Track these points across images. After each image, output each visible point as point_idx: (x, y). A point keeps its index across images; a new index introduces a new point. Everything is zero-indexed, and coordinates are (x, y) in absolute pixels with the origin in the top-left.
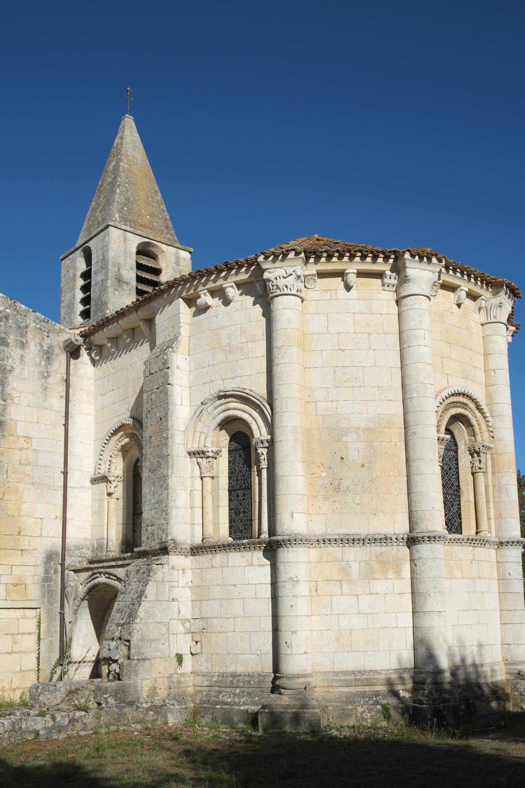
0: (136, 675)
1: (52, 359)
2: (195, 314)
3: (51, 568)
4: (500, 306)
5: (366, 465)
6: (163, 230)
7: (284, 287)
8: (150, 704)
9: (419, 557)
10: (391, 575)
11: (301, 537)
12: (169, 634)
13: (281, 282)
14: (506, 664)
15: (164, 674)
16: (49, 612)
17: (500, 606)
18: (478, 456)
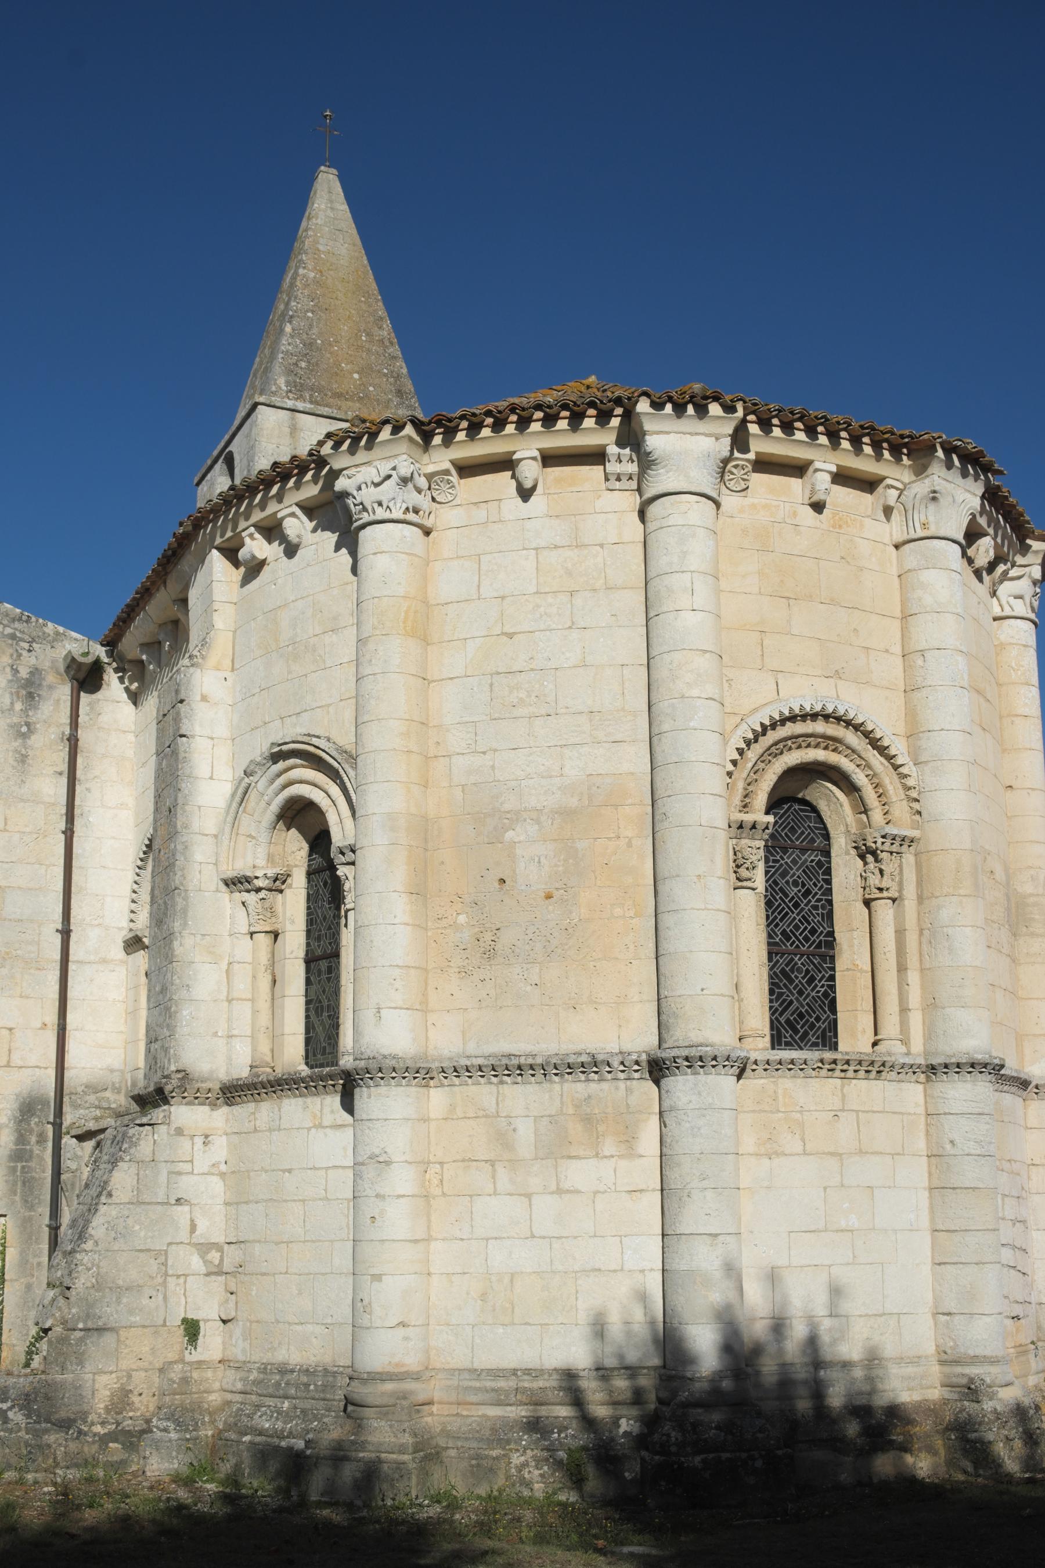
0: (81, 1363)
1: (39, 695)
2: (246, 580)
3: (31, 1131)
4: (934, 499)
5: (557, 894)
6: (390, 400)
7: (376, 506)
8: (114, 1426)
9: (671, 1106)
10: (609, 1147)
11: (393, 1063)
12: (166, 1274)
13: (368, 495)
14: (942, 1363)
15: (150, 1363)
16: (26, 1224)
17: (932, 1220)
18: (877, 860)
